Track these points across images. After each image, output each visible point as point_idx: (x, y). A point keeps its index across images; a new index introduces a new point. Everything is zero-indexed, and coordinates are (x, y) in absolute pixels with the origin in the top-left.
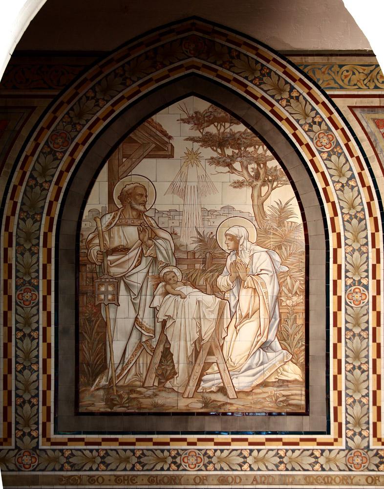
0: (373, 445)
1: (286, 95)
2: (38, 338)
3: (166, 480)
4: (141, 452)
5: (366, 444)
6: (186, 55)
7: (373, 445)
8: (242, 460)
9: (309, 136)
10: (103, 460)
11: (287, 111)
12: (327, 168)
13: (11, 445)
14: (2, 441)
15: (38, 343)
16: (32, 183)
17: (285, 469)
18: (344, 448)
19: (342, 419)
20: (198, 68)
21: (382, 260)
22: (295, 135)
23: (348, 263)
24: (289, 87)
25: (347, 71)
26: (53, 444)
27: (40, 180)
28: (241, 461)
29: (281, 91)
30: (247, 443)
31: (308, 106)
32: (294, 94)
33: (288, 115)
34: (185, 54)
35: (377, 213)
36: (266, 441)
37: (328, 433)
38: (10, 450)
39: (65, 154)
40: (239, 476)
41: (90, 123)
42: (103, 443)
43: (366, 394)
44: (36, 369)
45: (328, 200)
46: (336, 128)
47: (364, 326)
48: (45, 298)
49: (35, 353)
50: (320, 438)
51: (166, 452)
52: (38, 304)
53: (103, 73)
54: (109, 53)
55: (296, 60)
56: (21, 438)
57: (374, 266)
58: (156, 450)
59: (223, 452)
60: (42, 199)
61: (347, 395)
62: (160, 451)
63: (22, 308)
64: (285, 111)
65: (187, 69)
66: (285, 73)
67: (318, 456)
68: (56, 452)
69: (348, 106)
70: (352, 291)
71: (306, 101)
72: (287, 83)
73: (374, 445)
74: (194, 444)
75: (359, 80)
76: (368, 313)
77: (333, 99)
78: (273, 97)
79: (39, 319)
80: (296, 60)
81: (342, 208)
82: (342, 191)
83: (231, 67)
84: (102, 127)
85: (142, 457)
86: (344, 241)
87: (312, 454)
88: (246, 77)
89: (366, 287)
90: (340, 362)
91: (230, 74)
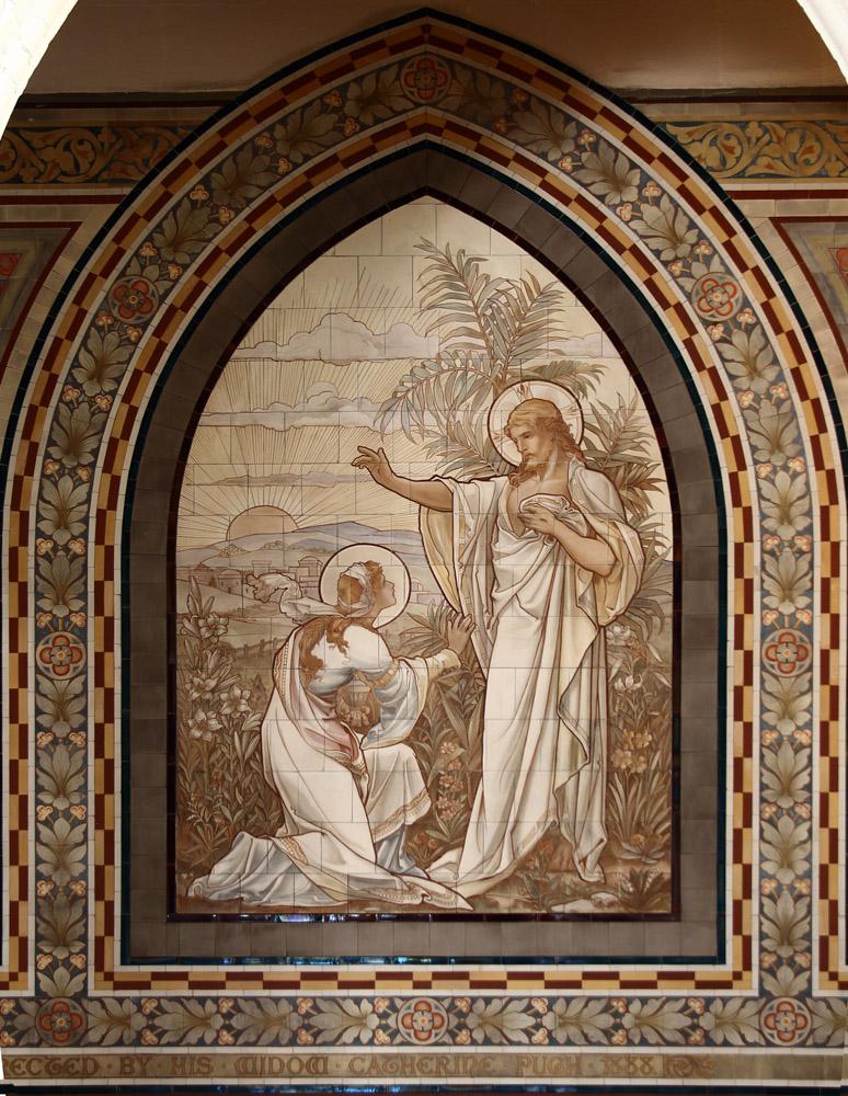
0: (95, 989)
1: (631, 195)
2: (86, 747)
3: (78, 1066)
4: (154, 1004)
5: (804, 986)
6: (412, 101)
7: (820, 989)
8: (531, 1021)
9: (682, 288)
10: (227, 1022)
11: (635, 231)
12: (723, 360)
13: (27, 989)
14: (6, 979)
15: (810, 758)
16: (72, 395)
17: (469, 1042)
18: (755, 993)
19: (752, 927)
20: (437, 131)
21: (843, 570)
22: (650, 284)
23: (44, 579)
24: (639, 176)
25: (807, 162)
26: (119, 986)
27: (91, 389)
28: (530, 1024)
29: (619, 184)
30: (467, 983)
31: (681, 218)
32: (651, 192)
33: (635, 239)
34: (408, 99)
35: (834, 460)
36: (377, 979)
37: (720, 958)
38: (747, 1000)
39: (144, 329)
40: (93, 1059)
41: (200, 260)
42: (429, 978)
43: (81, 874)
44: (805, 815)
45: (724, 433)
46: (743, 267)
47: (77, 720)
48: (99, 658)
49: (803, 779)
50: (703, 971)
51: (209, 1003)
52: (84, 672)
53: (225, 146)
54: (245, 97)
55: (653, 112)
56: (49, 971)
57: (825, 583)
58: (344, 998)
59: (490, 1003)
60: (92, 432)
61: (39, 876)
62: (351, 1002)
63: (51, 680)
64: (628, 229)
65: (416, 131)
66: (629, 142)
67: (698, 1011)
68: (124, 1005)
69: (771, 219)
70: (777, 640)
71: (677, 206)
72: (633, 166)
73: (822, 989)
74: (426, 985)
75: (703, 157)
76: (811, 689)
77: (737, 202)
78: (601, 198)
79: (86, 706)
80: (653, 112)
81: (754, 449)
82: (757, 411)
83: (510, 129)
84: (224, 272)
85: (313, 1015)
86: (758, 522)
87: (530, 1007)
88: (543, 153)
89: (82, 634)
90: (748, 798)
91: (509, 147)
